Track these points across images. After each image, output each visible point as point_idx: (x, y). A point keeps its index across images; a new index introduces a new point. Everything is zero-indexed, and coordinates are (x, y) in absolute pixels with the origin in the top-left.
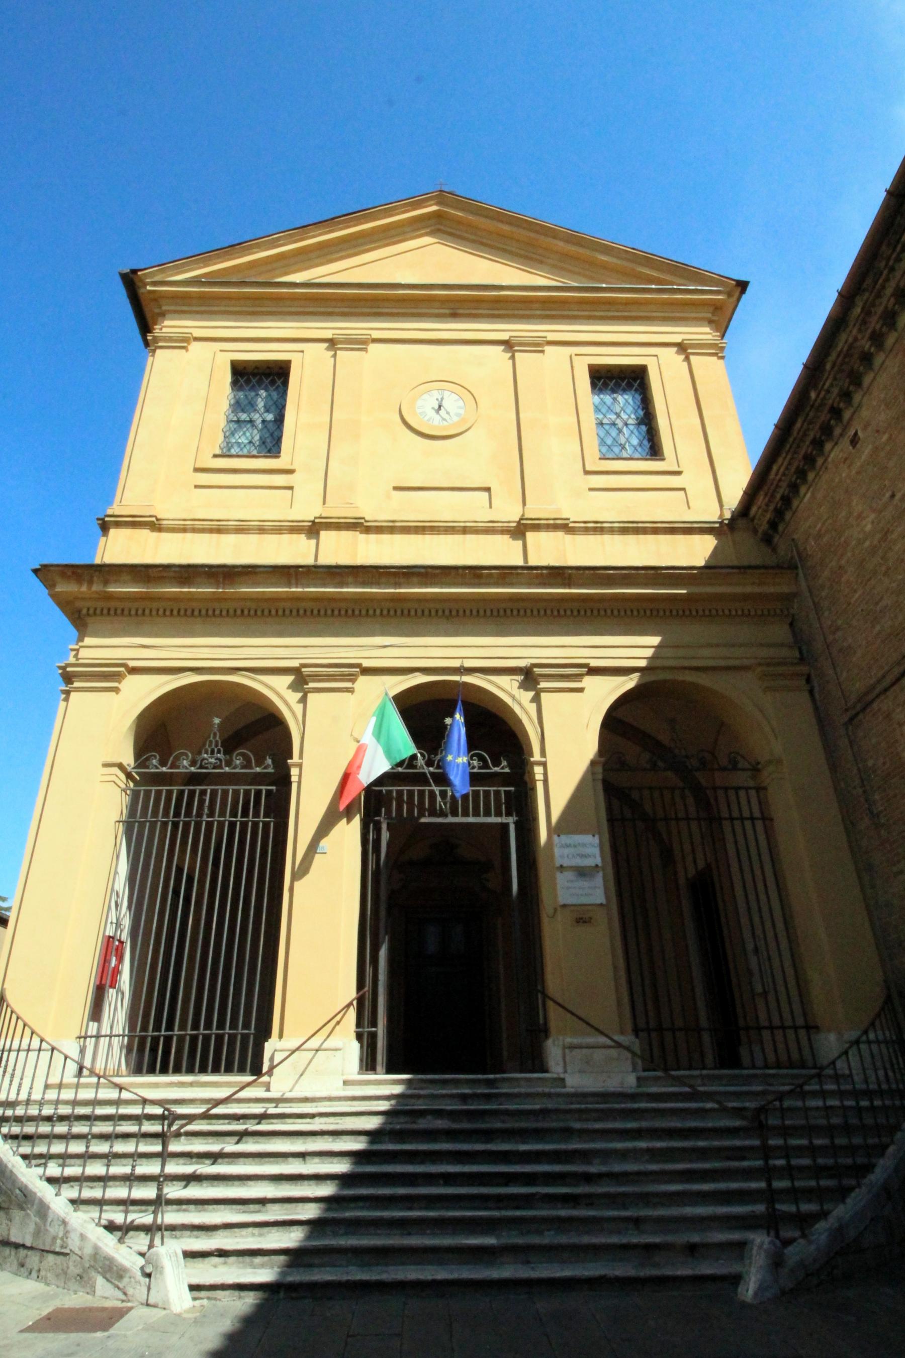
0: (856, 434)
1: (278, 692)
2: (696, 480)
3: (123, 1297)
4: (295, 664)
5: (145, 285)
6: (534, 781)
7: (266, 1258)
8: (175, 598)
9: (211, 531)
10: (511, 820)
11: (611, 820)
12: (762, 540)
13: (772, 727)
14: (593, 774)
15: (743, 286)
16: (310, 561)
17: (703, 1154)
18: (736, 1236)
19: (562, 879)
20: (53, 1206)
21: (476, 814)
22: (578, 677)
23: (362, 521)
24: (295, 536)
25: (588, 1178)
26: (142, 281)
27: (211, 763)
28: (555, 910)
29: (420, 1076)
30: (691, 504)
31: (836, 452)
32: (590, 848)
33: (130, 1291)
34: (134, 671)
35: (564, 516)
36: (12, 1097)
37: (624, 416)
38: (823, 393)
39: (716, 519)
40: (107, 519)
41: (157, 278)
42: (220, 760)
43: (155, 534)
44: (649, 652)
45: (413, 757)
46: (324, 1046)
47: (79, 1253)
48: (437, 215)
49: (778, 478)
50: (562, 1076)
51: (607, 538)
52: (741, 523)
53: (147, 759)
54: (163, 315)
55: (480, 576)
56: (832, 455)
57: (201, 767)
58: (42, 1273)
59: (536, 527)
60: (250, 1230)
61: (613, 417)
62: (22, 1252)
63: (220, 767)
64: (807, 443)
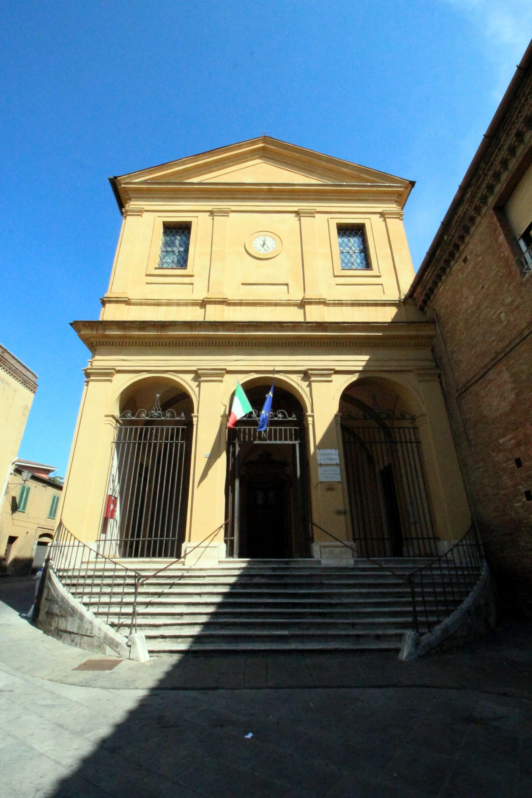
0: (466, 257)
2: (388, 280)
3: (119, 656)
4: (195, 368)
5: (121, 185)
7: (183, 639)
8: (139, 337)
9: (154, 305)
10: (297, 443)
11: (344, 442)
13: (421, 398)
14: (336, 421)
15: (413, 184)
16: (202, 319)
18: (398, 631)
19: (320, 470)
20: (86, 615)
21: (280, 439)
22: (329, 375)
24: (194, 307)
28: (317, 484)
32: (334, 455)
33: (122, 653)
34: (119, 372)
38: (450, 237)
39: (397, 299)
41: (127, 181)
43: (128, 306)
44: (364, 363)
45: (251, 413)
46: (210, 545)
48: (263, 148)
51: (344, 308)
52: (410, 301)
53: (126, 413)
54: (130, 199)
56: (454, 267)
57: (151, 417)
58: (82, 645)
60: (176, 627)
61: (348, 249)
62: (73, 636)
63: (160, 417)
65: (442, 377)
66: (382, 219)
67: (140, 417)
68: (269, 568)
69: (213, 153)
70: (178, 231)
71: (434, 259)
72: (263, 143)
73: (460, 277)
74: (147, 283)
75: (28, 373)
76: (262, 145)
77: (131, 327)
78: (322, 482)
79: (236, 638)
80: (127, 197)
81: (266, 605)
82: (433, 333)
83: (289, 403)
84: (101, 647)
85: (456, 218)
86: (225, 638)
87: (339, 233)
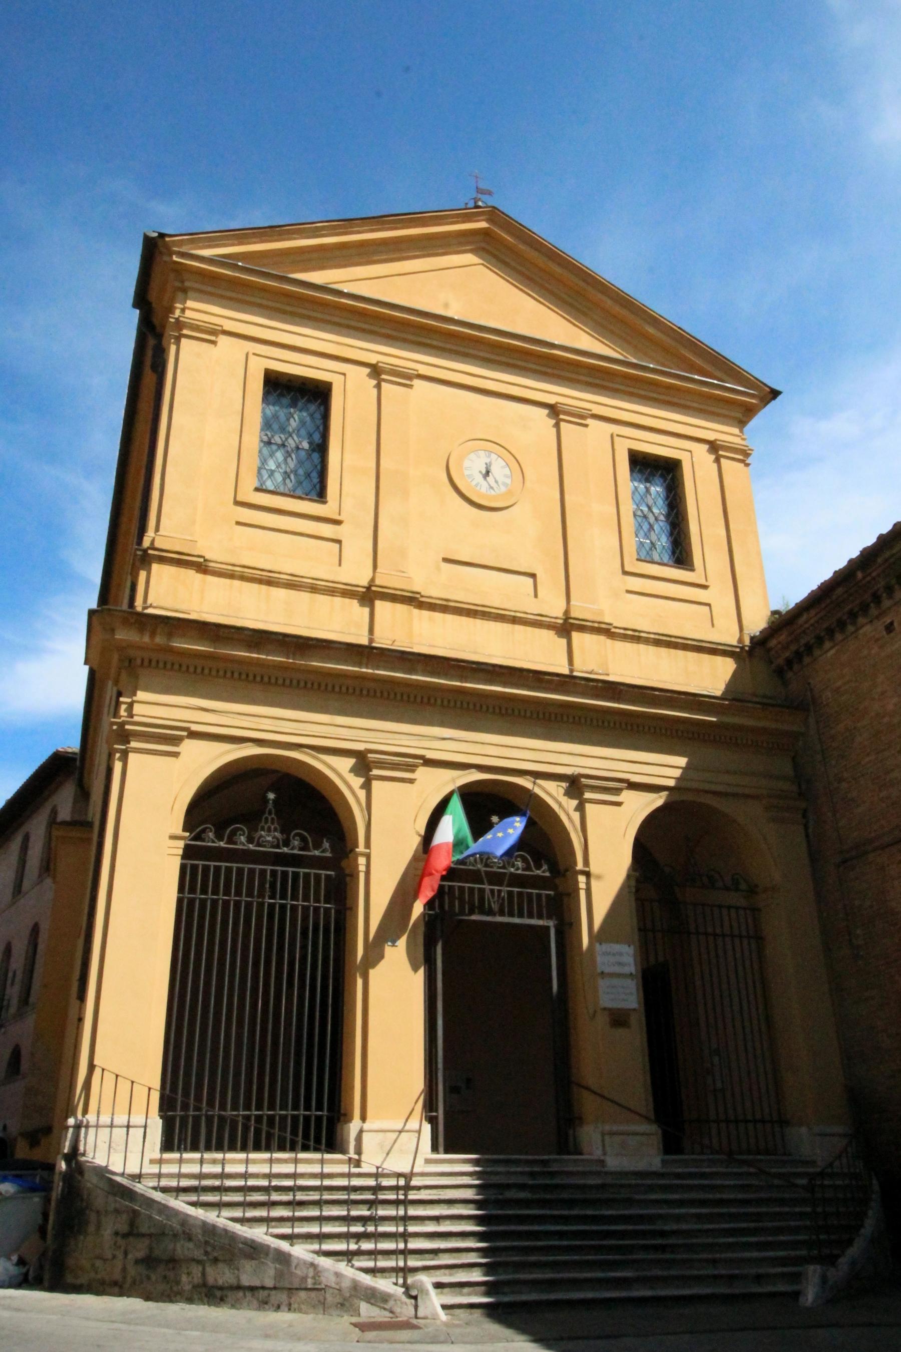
0: (892, 623)
1: (339, 771)
2: (719, 595)
3: (391, 1315)
4: (360, 747)
5: (171, 254)
6: (577, 890)
7: (471, 1289)
8: (241, 661)
10: (551, 923)
11: (642, 930)
13: (771, 851)
14: (629, 887)
19: (602, 984)
21: (521, 915)
22: (617, 791)
23: (418, 596)
24: (347, 601)
27: (269, 842)
29: (486, 1157)
30: (715, 622)
31: (869, 629)
32: (623, 958)
33: (397, 1310)
34: (193, 735)
35: (607, 621)
37: (656, 511)
38: (869, 578)
39: (735, 643)
40: (150, 552)
41: (183, 249)
42: (278, 840)
43: (200, 576)
44: (677, 773)
46: (407, 1128)
47: (337, 1287)
48: (485, 232)
49: (807, 626)
50: (602, 1158)
51: (642, 647)
53: (204, 831)
54: (185, 291)
55: (541, 681)
56: (864, 629)
57: (259, 845)
59: (582, 628)
60: (443, 1271)
61: (645, 509)
62: (262, 1294)
63: (278, 847)
66: (713, 457)
67: (235, 843)
68: (522, 1173)
69: (384, 223)
70: (298, 396)
71: (828, 601)
72: (487, 221)
73: (873, 652)
74: (238, 523)
76: (483, 225)
77: (232, 639)
78: (605, 1009)
79: (552, 1284)
83: (547, 846)
84: (347, 1304)
85: (887, 554)
86: (535, 1284)
87: (632, 470)
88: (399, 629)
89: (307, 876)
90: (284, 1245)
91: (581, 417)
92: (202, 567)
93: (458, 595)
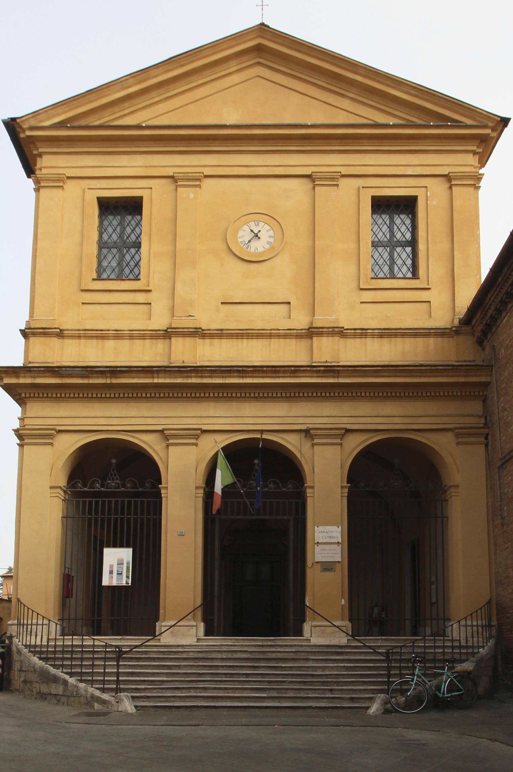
1: (291, 443)
2: (438, 297)
5: (24, 131)
9: (97, 337)
12: (477, 342)
15: (505, 122)
16: (165, 364)
17: (370, 668)
18: (371, 696)
19: (317, 549)
20: (69, 681)
23: (200, 330)
25: (312, 676)
26: (21, 127)
27: (113, 486)
28: (313, 564)
35: (340, 326)
36: (33, 643)
42: (118, 484)
43: (342, 341)
45: (234, 483)
50: (309, 638)
52: (464, 328)
53: (76, 483)
54: (40, 155)
57: (107, 488)
58: (70, 703)
62: (59, 697)
63: (118, 488)
64: (509, 284)
65: (490, 438)
67: (94, 488)
70: (119, 210)
75: (223, 647)
78: (318, 562)
80: (35, 152)
81: (247, 675)
82: (488, 379)
84: (89, 703)
88: (184, 352)
89: (148, 502)
90: (67, 677)
91: (333, 179)
92: (61, 334)
93: (232, 325)
